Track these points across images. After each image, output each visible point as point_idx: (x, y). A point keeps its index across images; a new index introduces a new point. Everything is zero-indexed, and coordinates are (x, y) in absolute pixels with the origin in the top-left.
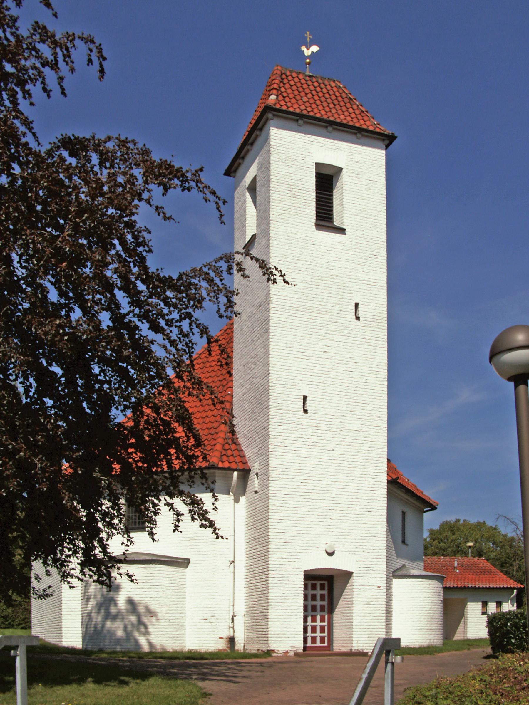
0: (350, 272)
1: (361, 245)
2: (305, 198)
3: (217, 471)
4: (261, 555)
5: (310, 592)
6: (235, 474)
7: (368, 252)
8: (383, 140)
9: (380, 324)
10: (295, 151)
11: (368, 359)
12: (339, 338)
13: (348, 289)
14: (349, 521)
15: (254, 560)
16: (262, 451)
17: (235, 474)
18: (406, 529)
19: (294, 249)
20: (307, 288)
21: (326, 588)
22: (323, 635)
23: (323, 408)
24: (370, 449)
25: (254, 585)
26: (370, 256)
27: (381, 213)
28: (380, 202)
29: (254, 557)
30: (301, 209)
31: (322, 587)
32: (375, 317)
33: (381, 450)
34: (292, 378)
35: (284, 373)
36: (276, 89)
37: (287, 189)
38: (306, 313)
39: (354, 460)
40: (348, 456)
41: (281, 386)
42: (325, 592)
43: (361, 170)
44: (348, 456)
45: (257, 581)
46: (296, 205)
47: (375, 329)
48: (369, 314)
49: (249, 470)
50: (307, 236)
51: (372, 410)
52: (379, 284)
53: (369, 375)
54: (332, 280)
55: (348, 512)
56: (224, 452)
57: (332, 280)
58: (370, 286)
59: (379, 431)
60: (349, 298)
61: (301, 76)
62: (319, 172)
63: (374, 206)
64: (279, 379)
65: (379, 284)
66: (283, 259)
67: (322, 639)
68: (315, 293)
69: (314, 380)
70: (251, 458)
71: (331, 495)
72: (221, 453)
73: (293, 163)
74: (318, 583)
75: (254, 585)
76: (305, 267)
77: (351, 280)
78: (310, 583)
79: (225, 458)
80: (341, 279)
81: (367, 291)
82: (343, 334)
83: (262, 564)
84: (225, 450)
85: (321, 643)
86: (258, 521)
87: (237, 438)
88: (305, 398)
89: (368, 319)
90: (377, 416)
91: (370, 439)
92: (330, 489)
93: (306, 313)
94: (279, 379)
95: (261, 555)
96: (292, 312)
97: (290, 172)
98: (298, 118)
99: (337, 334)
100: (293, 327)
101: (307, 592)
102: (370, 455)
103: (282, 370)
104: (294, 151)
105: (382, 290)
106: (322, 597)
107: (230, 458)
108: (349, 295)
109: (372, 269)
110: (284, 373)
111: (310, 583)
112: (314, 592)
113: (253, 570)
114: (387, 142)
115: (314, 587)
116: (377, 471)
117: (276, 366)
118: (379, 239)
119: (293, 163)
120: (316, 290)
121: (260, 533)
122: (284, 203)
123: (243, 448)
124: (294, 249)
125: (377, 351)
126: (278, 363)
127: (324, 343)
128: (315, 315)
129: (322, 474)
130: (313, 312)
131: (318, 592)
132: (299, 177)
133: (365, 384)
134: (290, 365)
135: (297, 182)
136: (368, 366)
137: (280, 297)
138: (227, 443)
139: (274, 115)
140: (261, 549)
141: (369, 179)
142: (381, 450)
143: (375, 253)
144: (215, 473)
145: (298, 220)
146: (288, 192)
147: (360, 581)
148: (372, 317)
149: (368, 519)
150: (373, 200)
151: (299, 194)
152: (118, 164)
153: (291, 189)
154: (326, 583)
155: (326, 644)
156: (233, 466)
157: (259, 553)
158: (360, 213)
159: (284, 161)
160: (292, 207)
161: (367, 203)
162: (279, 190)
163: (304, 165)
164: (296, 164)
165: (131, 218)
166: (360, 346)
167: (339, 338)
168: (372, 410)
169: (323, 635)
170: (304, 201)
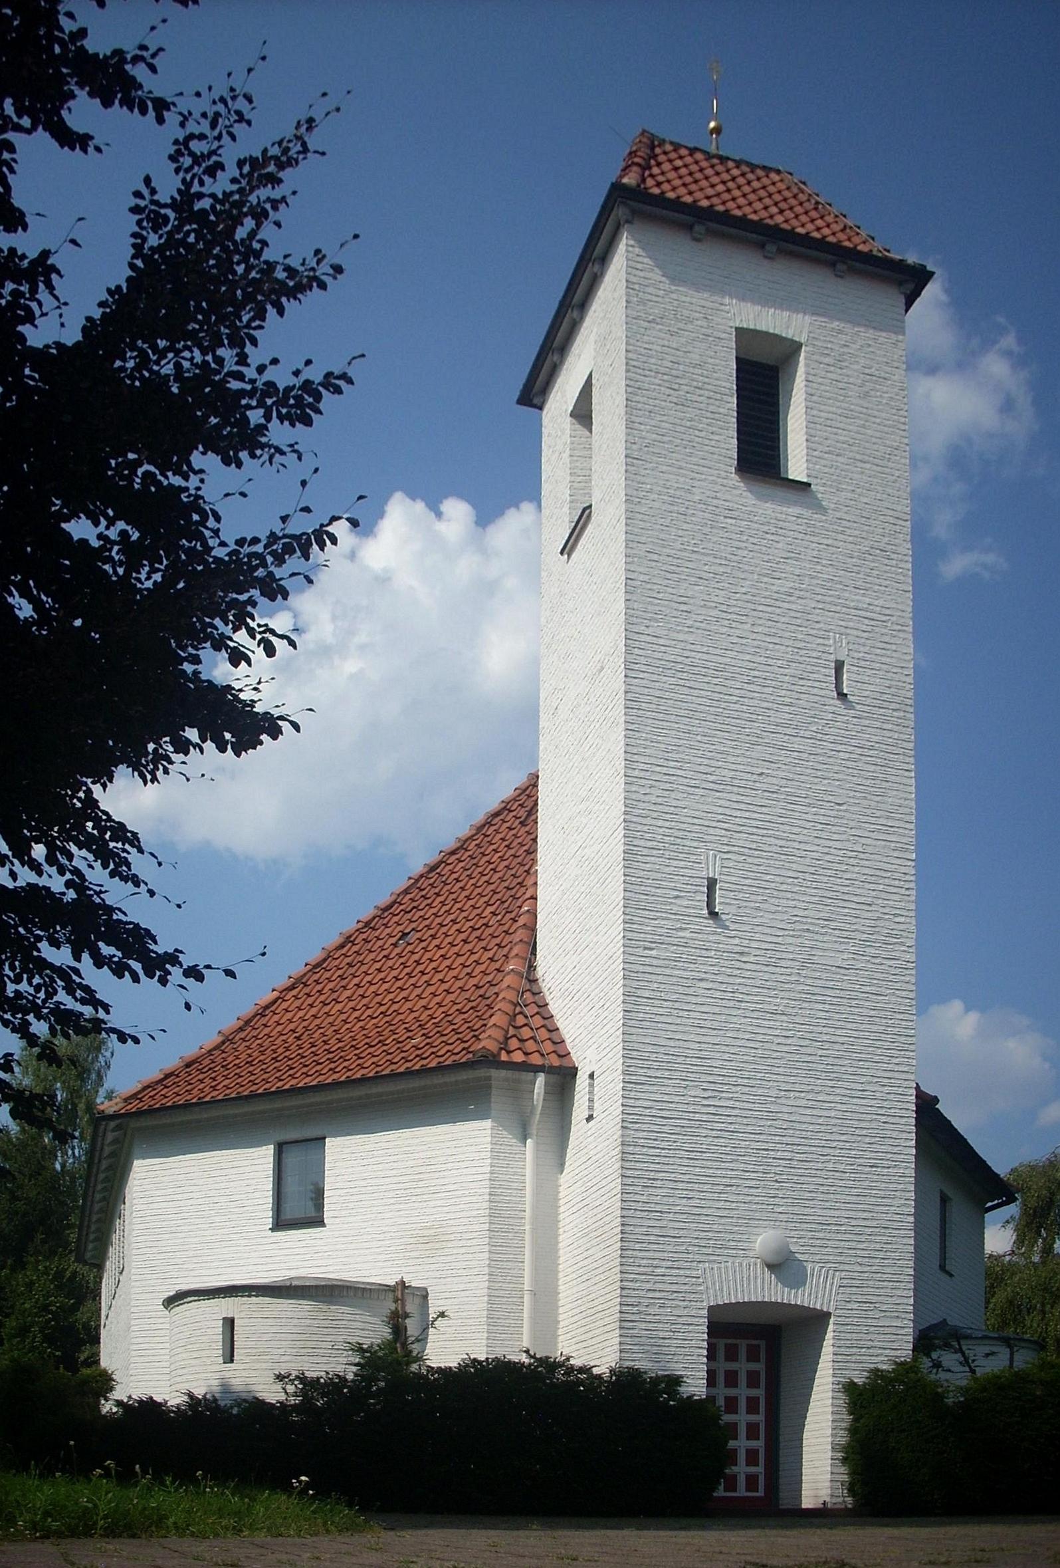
0: (823, 586)
1: (848, 524)
2: (711, 408)
3: (494, 1073)
4: (601, 1270)
5: (723, 1366)
6: (541, 1079)
7: (866, 543)
8: (900, 284)
9: (895, 714)
10: (688, 299)
11: (869, 797)
12: (797, 744)
13: (818, 626)
14: (821, 1188)
15: (582, 1287)
16: (606, 1013)
17: (541, 1079)
18: (937, 1225)
19: (685, 526)
20: (718, 619)
21: (763, 1355)
22: (752, 1469)
23: (758, 909)
24: (872, 1013)
25: (584, 1345)
26: (872, 551)
27: (896, 452)
28: (893, 427)
29: (585, 1277)
30: (703, 434)
31: (753, 1356)
32: (885, 697)
33: (901, 1016)
34: (680, 834)
35: (660, 823)
36: (638, 165)
37: (667, 385)
38: (716, 681)
39: (834, 1039)
40: (820, 1029)
41: (655, 852)
42: (760, 1367)
43: (846, 350)
44: (820, 1029)
45: (590, 1335)
46: (688, 424)
47: (885, 726)
48: (871, 688)
49: (573, 1072)
50: (716, 498)
51: (879, 919)
52: (894, 619)
53: (871, 835)
54: (778, 604)
55: (820, 1166)
56: (512, 1031)
57: (778, 604)
58: (872, 623)
59: (897, 971)
60: (821, 648)
61: (699, 156)
62: (743, 356)
63: (878, 434)
64: (647, 836)
65: (894, 619)
66: (657, 549)
67: (752, 1481)
68: (738, 632)
69: (734, 842)
70: (577, 1041)
71: (778, 1123)
72: (507, 1032)
73: (681, 325)
74: (743, 1345)
75: (584, 1345)
76: (713, 569)
77: (828, 607)
78: (721, 1343)
79: (514, 1044)
80: (800, 601)
81: (865, 635)
82: (807, 734)
83: (603, 1292)
84: (515, 1027)
85: (748, 1490)
86: (595, 1188)
87: (547, 1004)
88: (712, 884)
89: (868, 701)
90: (889, 935)
91: (873, 989)
92: (773, 1108)
93: (716, 681)
94: (647, 836)
95: (601, 1270)
96: (679, 675)
97: (674, 345)
98: (689, 219)
99: (793, 732)
100: (682, 712)
101: (714, 1365)
102: (874, 1028)
103: (655, 815)
104: (684, 299)
105: (901, 635)
106: (753, 1380)
107: (527, 1043)
108: (821, 641)
109: (877, 581)
110: (660, 823)
111: (721, 1343)
112: (733, 1366)
113: (583, 1308)
114: (910, 287)
115: (732, 1355)
116: (890, 1067)
117: (641, 805)
118: (891, 513)
119: (681, 325)
120: (740, 626)
121: (599, 1216)
122: (659, 418)
123: (559, 1025)
124: (685, 526)
125: (890, 778)
126: (646, 798)
127: (758, 752)
128: (738, 685)
129: (755, 1070)
130: (733, 679)
131: (743, 1367)
132: (695, 357)
133: (862, 856)
134: (674, 803)
135: (691, 370)
136: (869, 812)
137: (648, 639)
138: (521, 1013)
139: (634, 212)
140: (600, 1255)
141: (867, 371)
142: (901, 1016)
143: (882, 545)
144: (489, 1078)
145: (694, 460)
146: (669, 391)
147: (848, 1336)
148: (878, 695)
149: (867, 1183)
150: (878, 421)
151: (695, 398)
152: (261, 369)
153: (676, 387)
154: (763, 1344)
155: (761, 1493)
156: (536, 1059)
157: (595, 1265)
158: (844, 449)
159: (658, 320)
160: (678, 429)
161: (864, 426)
162: (647, 386)
163: (709, 331)
164: (690, 327)
165: (264, 422)
166: (849, 764)
167: (797, 744)
168: (879, 919)
169: (752, 1469)
170: (709, 415)
